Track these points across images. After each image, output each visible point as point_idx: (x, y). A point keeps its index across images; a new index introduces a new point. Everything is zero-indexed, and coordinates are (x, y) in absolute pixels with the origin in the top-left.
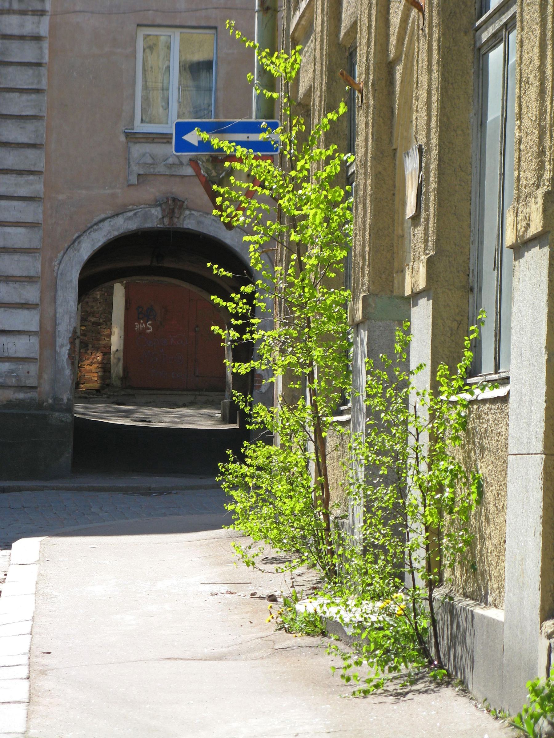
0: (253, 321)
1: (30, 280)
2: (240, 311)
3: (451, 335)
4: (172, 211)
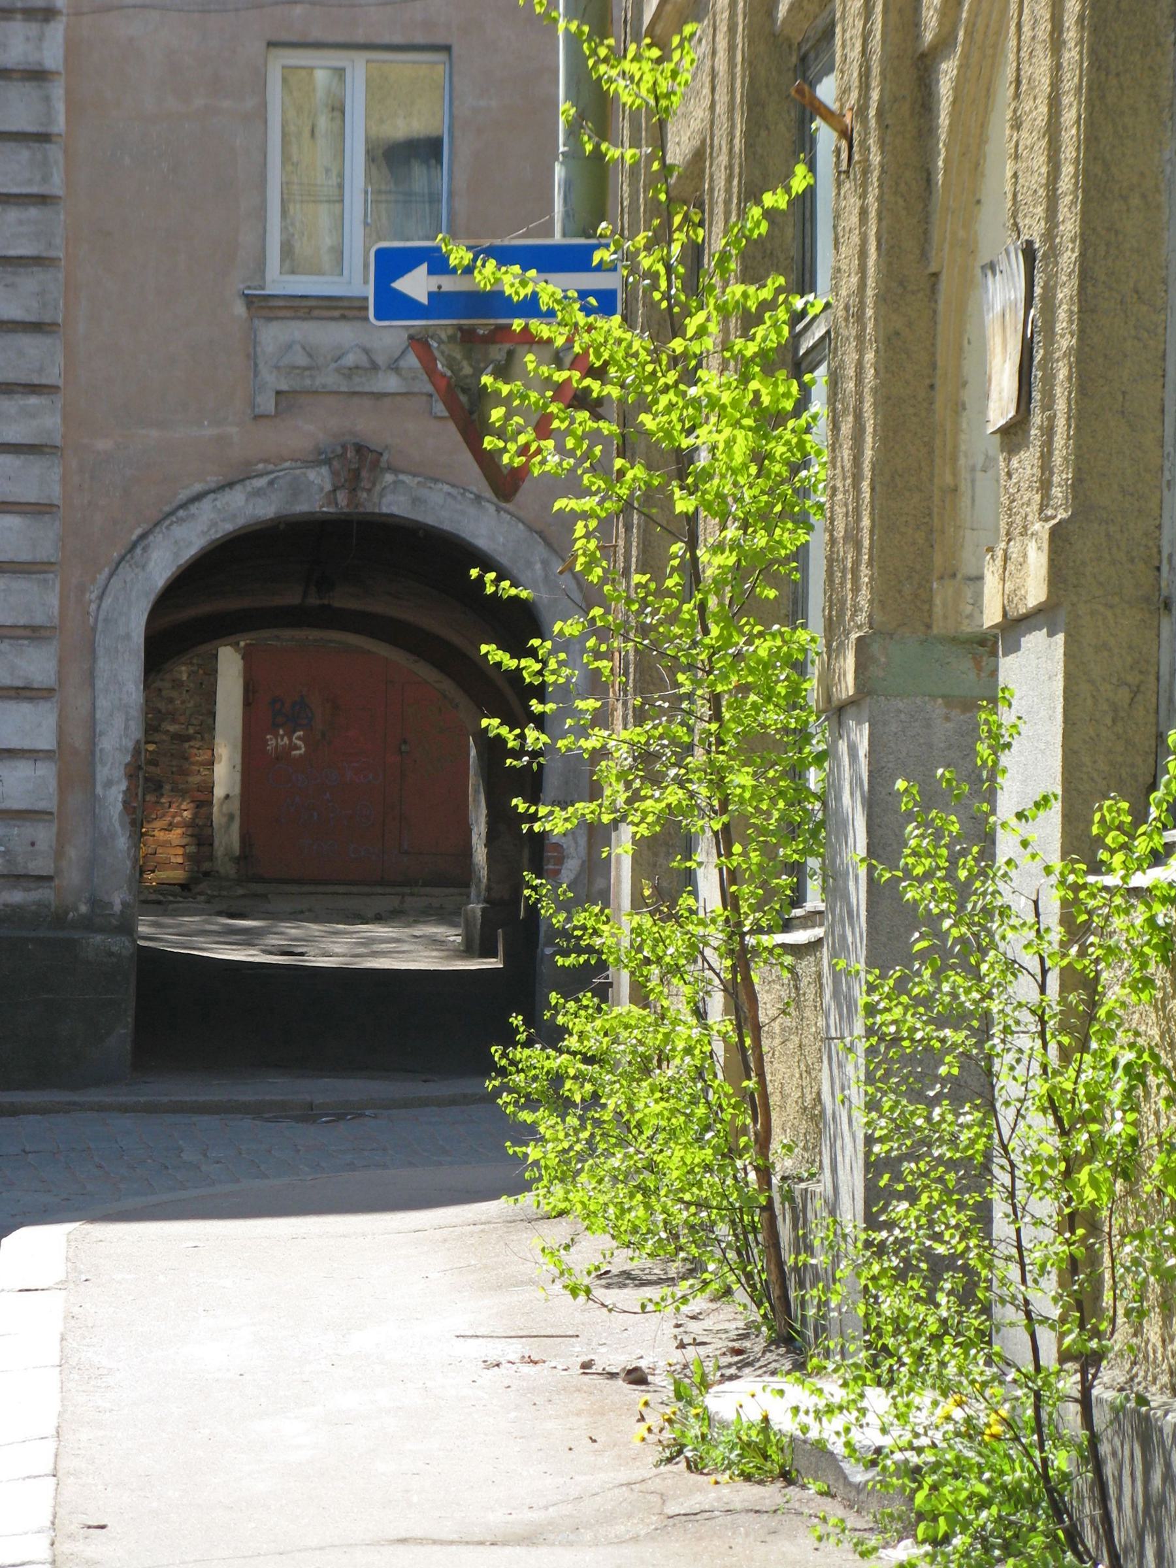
0: (581, 704)
1: (34, 633)
2: (551, 679)
3: (1114, 721)
4: (356, 475)
